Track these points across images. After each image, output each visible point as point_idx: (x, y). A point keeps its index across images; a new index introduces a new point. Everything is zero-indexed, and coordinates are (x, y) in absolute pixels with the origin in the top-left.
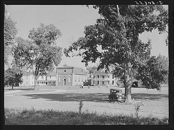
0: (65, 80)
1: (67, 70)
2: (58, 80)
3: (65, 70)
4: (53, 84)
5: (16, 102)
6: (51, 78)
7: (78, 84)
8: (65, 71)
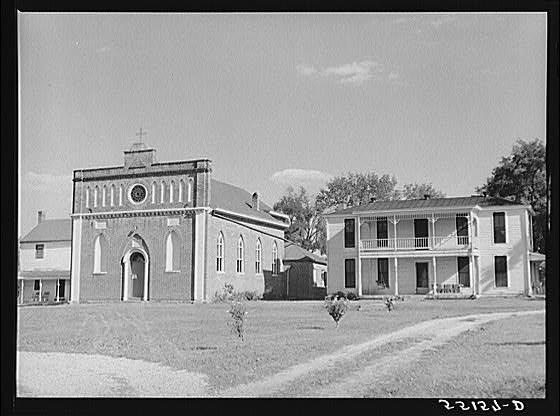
0: (137, 257)
1: (150, 185)
2: (87, 261)
3: (133, 183)
4: (53, 290)
5: (40, 374)
6: (40, 256)
7: (239, 288)
8: (139, 194)
